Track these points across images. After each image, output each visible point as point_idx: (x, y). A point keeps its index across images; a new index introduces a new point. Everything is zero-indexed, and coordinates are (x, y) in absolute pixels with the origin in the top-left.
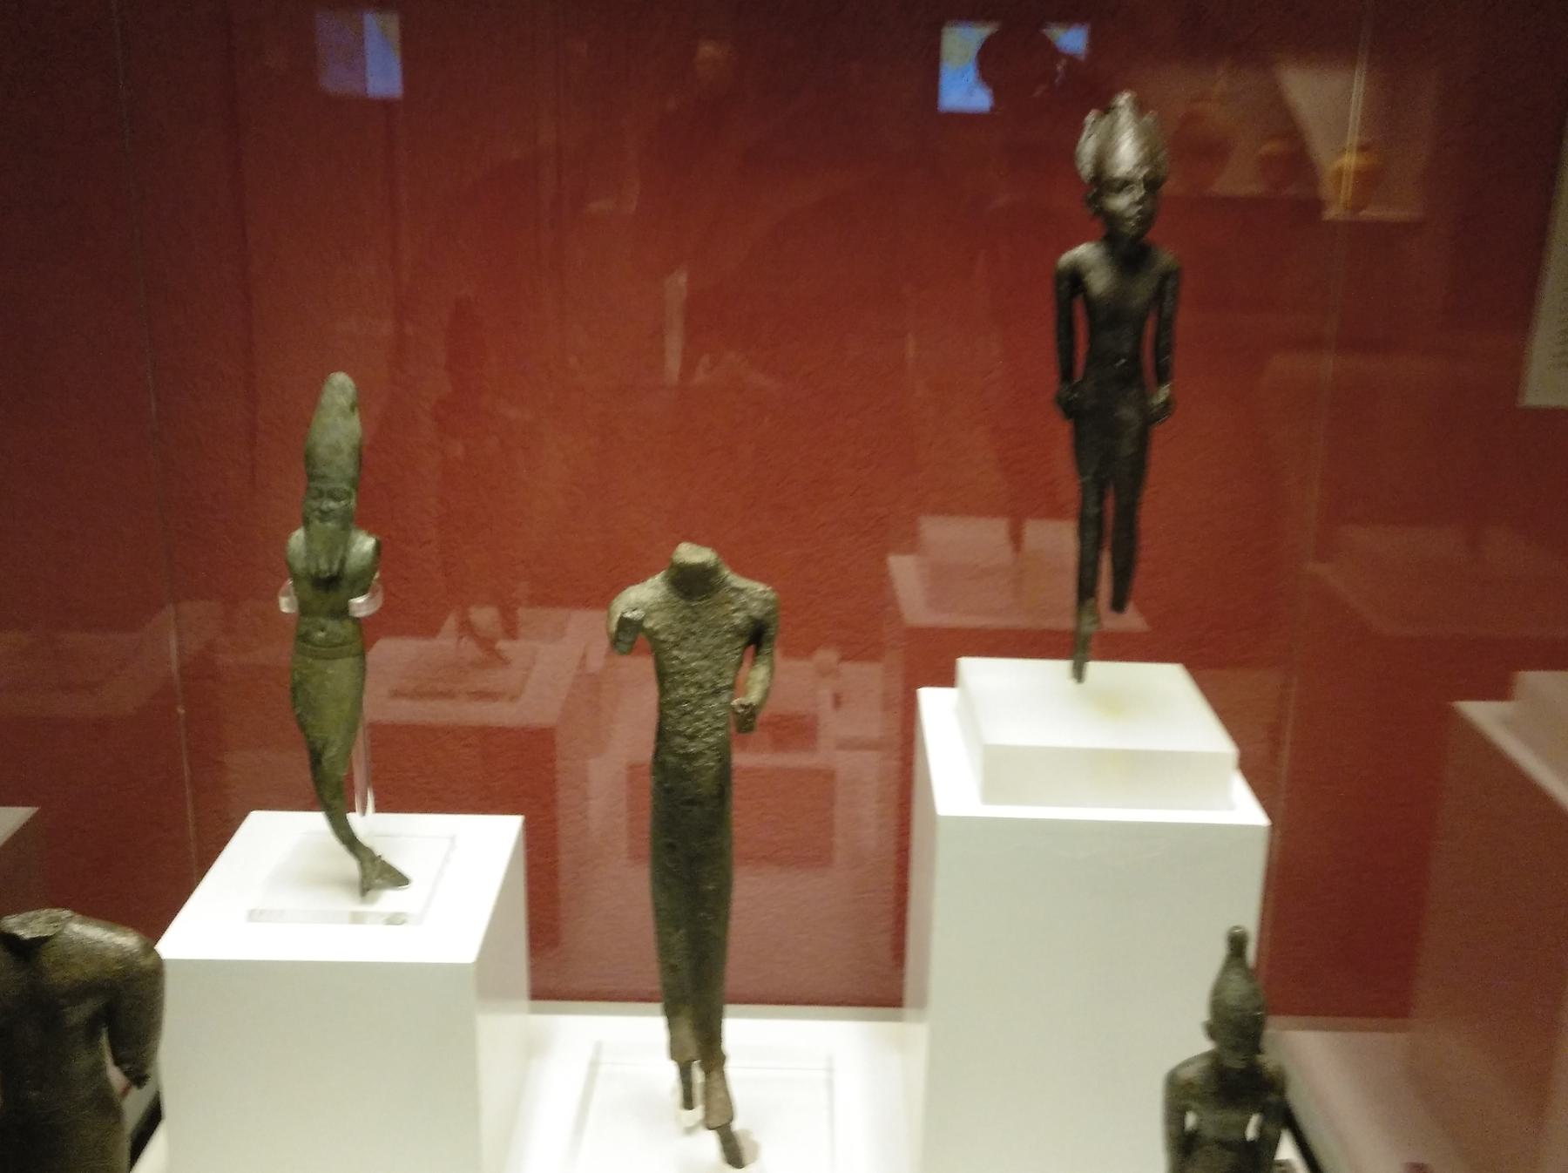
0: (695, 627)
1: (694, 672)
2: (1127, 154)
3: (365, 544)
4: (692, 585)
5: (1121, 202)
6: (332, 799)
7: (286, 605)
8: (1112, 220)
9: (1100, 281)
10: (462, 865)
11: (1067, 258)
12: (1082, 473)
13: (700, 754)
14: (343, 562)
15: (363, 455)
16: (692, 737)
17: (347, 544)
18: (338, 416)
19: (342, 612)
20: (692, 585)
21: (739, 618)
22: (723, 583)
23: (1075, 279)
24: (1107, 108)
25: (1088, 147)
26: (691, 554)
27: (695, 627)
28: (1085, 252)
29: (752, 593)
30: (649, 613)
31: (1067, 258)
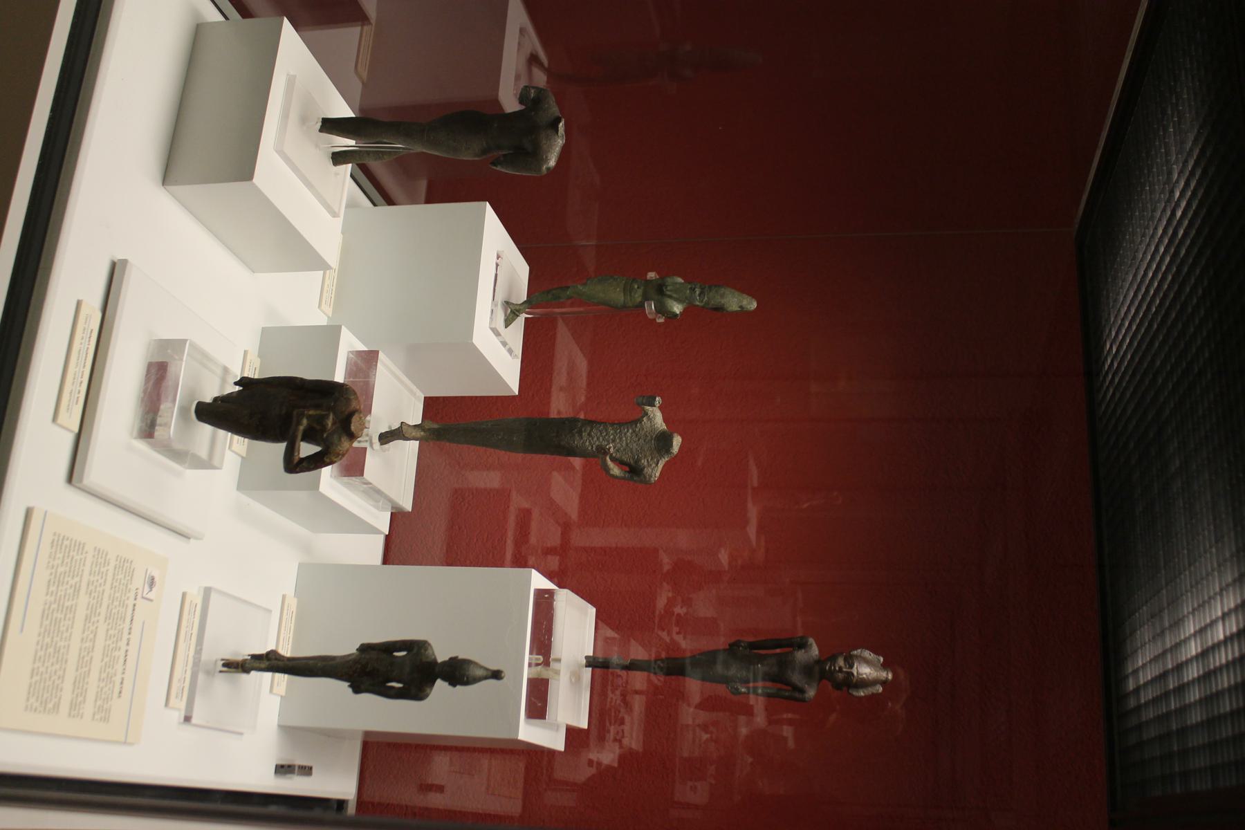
0: (641, 441)
1: (621, 439)
2: (864, 671)
3: (677, 308)
4: (663, 441)
5: (841, 662)
6: (530, 303)
7: (652, 275)
8: (833, 658)
9: (800, 655)
10: (500, 358)
11: (811, 640)
12: (702, 654)
13: (581, 436)
14: (670, 297)
15: (719, 309)
16: (589, 435)
17: (679, 300)
18: (737, 302)
19: (646, 297)
20: (663, 441)
21: (644, 462)
22: (662, 456)
23: (802, 645)
24: (885, 666)
25: (867, 654)
26: (677, 441)
27: (641, 441)
28: (815, 651)
29: (655, 471)
30: (649, 419)
31: (811, 640)
